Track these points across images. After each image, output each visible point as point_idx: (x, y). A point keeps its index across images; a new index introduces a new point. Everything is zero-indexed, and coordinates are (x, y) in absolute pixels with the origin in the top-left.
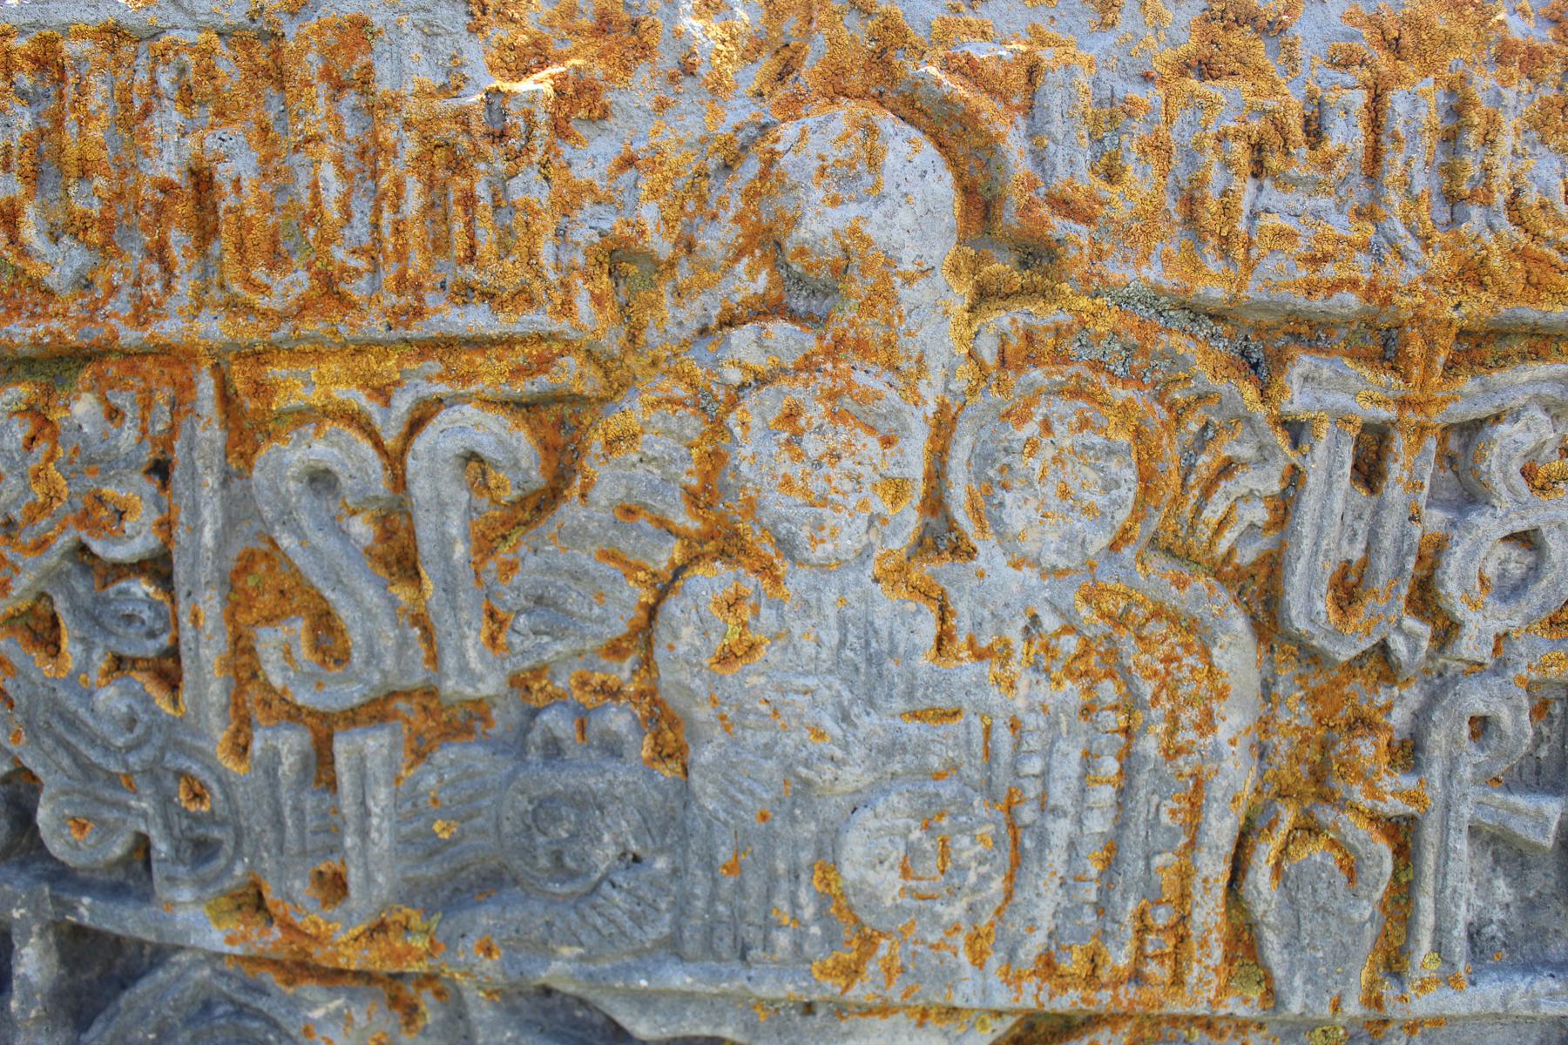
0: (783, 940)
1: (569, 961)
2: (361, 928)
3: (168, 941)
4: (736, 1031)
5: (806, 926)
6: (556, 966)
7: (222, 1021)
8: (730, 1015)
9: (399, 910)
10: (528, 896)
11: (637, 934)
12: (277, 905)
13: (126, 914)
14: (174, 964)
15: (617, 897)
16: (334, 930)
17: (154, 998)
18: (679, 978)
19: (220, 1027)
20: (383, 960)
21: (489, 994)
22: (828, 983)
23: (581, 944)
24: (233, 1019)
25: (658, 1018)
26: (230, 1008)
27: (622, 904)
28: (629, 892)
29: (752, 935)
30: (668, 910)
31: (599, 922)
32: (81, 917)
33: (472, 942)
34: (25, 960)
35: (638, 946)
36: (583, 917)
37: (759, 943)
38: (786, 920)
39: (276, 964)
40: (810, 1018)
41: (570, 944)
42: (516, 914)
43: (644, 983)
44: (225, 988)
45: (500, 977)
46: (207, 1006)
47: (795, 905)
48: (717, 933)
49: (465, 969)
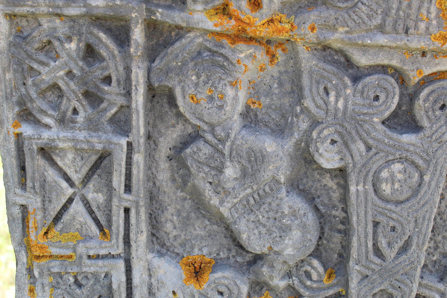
0: (422, 26)
1: (342, 33)
2: (266, 20)
3: (191, 26)
4: (398, 62)
5: (431, 20)
6: (337, 35)
7: (207, 58)
8: (395, 56)
9: (278, 15)
10: (328, 8)
11: (369, 23)
12: (235, 11)
13: (175, 16)
14: (188, 37)
15: (364, 8)
16: (256, 21)
17: (180, 50)
18: (382, 40)
19: (206, 60)
20: (273, 32)
21: (307, 48)
22: (437, 43)
23: (348, 26)
24: (211, 57)
25: (369, 57)
26: (209, 54)
27: (365, 11)
28: (368, 6)
29: (411, 24)
30: (380, 14)
31: (356, 18)
32: (157, 17)
33: (308, 25)
34: (136, 33)
35: (368, 27)
36: (350, 16)
37: (413, 27)
38: (425, 18)
39: (228, 36)
40: (424, 58)
41: (344, 27)
42: (325, 14)
43: (369, 42)
44: (208, 45)
45: (315, 40)
46: (199, 53)
47: (429, 12)
48: (398, 23)
49: (303, 37)
